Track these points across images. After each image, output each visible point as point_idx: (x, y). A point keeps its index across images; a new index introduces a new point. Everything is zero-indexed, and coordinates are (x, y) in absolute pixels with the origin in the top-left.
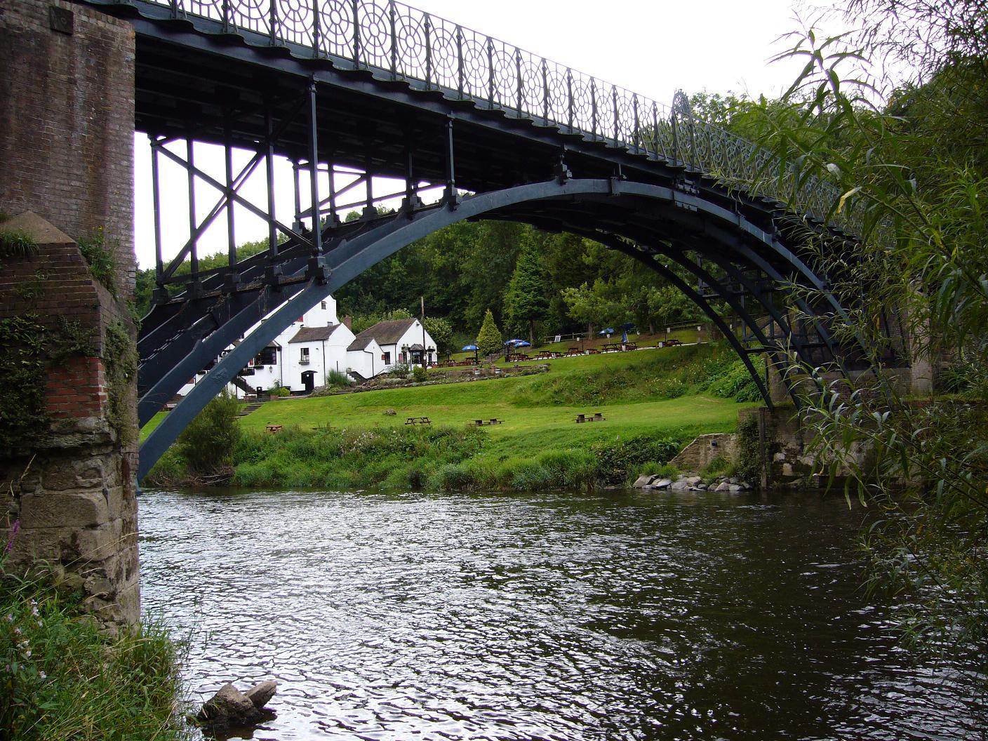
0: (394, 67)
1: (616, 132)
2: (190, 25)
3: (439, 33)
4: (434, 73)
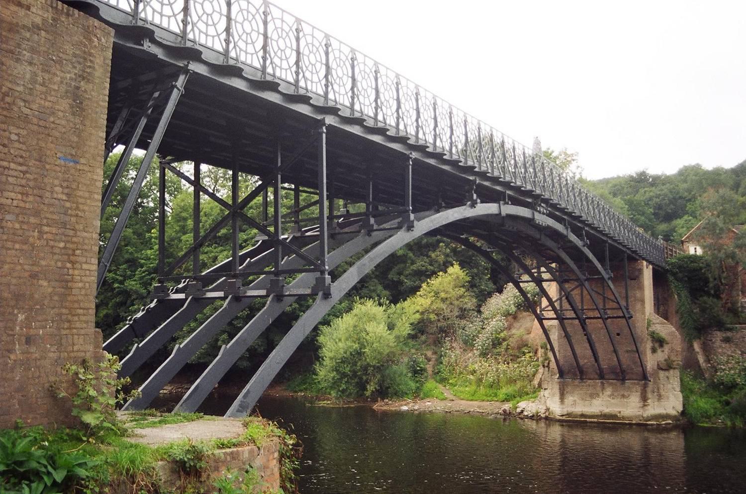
0: (184, 32)
1: (376, 110)
2: (241, 70)
3: (309, 39)
4: (235, 47)
